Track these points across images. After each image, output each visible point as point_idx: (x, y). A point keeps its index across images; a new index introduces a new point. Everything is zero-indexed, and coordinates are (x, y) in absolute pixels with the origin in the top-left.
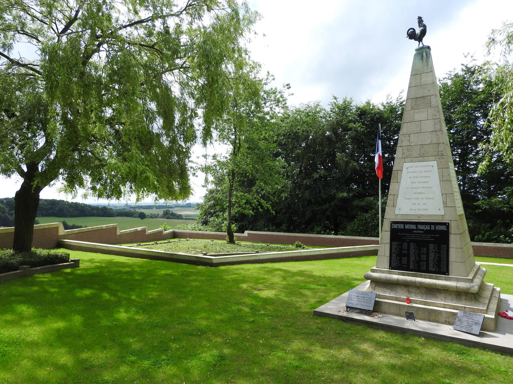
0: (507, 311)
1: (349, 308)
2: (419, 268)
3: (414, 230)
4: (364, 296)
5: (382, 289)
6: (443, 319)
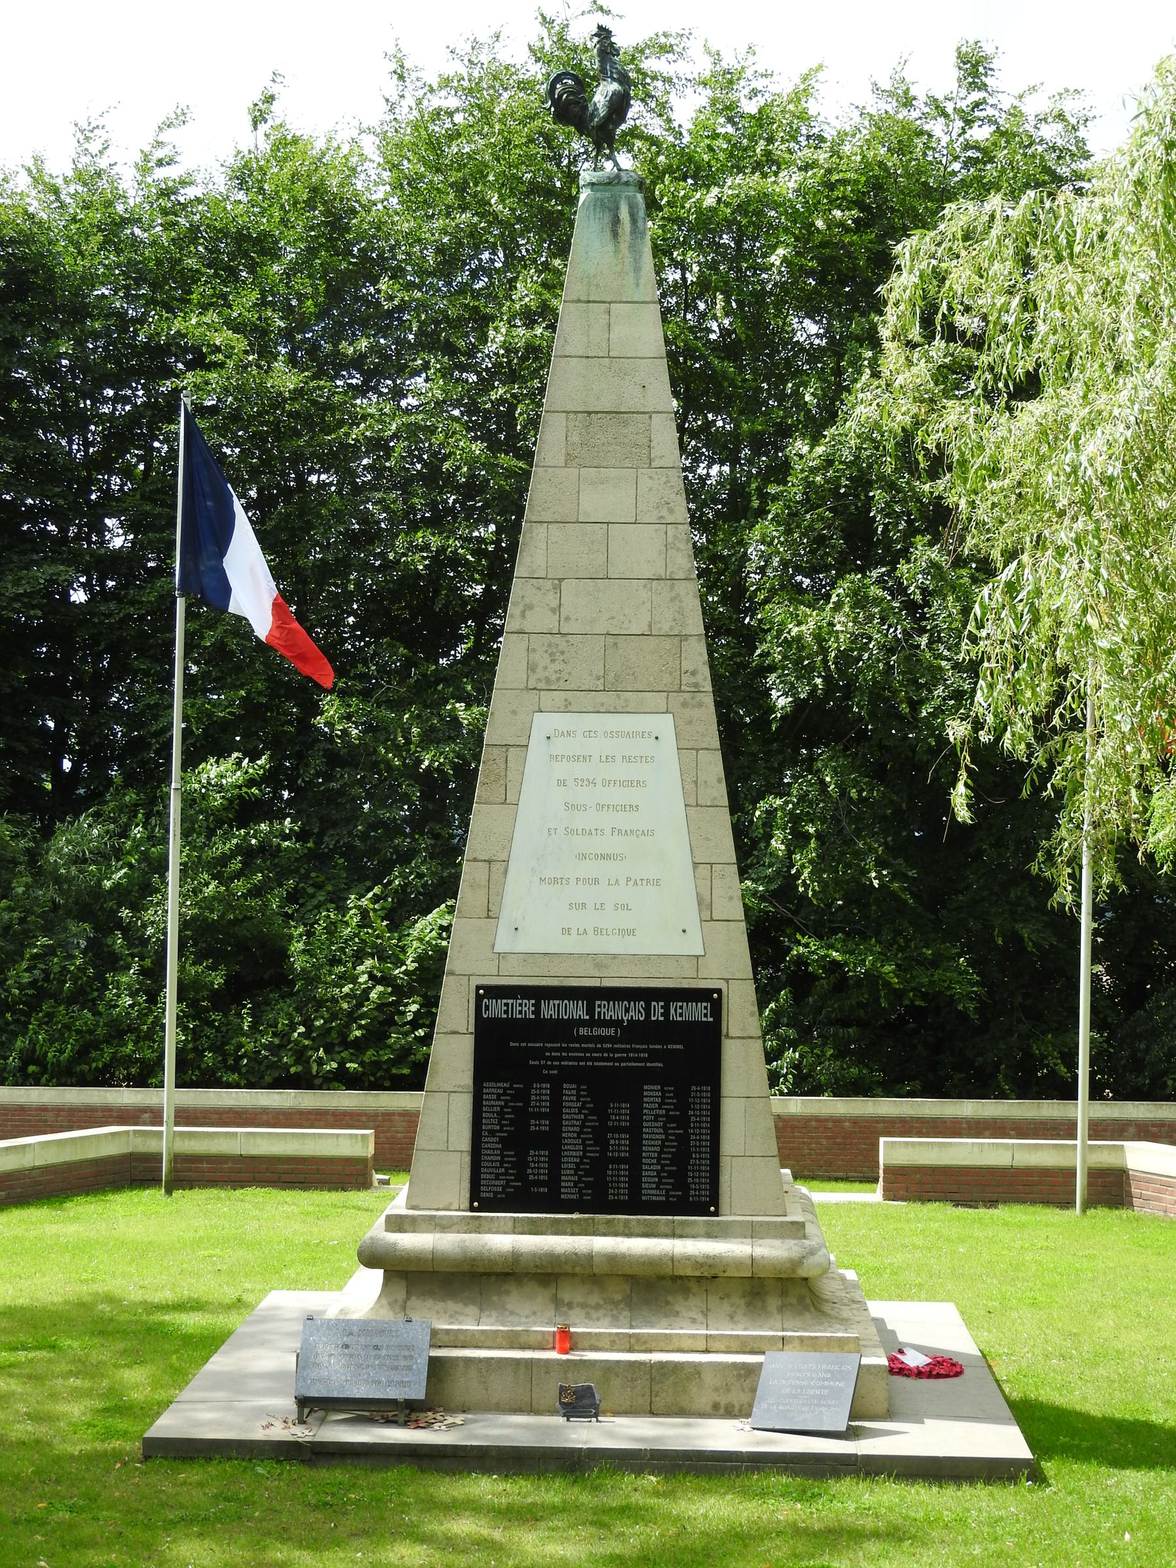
0: (901, 1352)
1: (310, 1406)
2: (604, 1194)
3: (581, 1023)
4: (376, 1341)
5: (440, 1306)
6: (703, 1401)
